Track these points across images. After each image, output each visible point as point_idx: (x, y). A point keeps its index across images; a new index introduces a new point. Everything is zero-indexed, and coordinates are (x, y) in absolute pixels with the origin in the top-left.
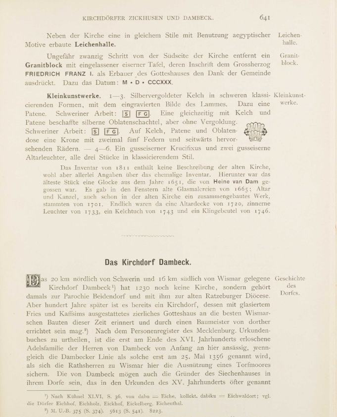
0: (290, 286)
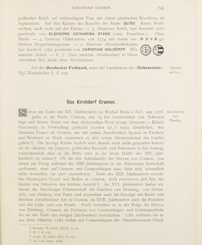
0: (174, 116)
